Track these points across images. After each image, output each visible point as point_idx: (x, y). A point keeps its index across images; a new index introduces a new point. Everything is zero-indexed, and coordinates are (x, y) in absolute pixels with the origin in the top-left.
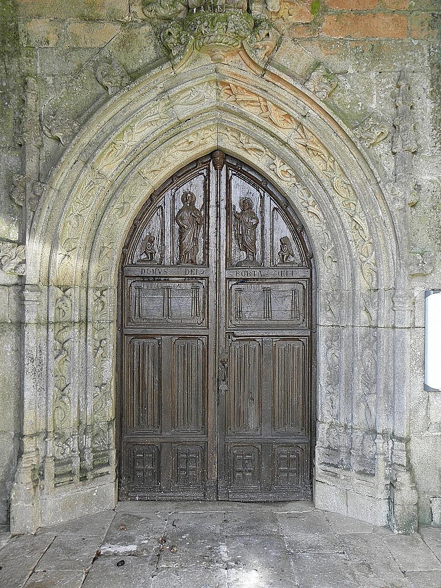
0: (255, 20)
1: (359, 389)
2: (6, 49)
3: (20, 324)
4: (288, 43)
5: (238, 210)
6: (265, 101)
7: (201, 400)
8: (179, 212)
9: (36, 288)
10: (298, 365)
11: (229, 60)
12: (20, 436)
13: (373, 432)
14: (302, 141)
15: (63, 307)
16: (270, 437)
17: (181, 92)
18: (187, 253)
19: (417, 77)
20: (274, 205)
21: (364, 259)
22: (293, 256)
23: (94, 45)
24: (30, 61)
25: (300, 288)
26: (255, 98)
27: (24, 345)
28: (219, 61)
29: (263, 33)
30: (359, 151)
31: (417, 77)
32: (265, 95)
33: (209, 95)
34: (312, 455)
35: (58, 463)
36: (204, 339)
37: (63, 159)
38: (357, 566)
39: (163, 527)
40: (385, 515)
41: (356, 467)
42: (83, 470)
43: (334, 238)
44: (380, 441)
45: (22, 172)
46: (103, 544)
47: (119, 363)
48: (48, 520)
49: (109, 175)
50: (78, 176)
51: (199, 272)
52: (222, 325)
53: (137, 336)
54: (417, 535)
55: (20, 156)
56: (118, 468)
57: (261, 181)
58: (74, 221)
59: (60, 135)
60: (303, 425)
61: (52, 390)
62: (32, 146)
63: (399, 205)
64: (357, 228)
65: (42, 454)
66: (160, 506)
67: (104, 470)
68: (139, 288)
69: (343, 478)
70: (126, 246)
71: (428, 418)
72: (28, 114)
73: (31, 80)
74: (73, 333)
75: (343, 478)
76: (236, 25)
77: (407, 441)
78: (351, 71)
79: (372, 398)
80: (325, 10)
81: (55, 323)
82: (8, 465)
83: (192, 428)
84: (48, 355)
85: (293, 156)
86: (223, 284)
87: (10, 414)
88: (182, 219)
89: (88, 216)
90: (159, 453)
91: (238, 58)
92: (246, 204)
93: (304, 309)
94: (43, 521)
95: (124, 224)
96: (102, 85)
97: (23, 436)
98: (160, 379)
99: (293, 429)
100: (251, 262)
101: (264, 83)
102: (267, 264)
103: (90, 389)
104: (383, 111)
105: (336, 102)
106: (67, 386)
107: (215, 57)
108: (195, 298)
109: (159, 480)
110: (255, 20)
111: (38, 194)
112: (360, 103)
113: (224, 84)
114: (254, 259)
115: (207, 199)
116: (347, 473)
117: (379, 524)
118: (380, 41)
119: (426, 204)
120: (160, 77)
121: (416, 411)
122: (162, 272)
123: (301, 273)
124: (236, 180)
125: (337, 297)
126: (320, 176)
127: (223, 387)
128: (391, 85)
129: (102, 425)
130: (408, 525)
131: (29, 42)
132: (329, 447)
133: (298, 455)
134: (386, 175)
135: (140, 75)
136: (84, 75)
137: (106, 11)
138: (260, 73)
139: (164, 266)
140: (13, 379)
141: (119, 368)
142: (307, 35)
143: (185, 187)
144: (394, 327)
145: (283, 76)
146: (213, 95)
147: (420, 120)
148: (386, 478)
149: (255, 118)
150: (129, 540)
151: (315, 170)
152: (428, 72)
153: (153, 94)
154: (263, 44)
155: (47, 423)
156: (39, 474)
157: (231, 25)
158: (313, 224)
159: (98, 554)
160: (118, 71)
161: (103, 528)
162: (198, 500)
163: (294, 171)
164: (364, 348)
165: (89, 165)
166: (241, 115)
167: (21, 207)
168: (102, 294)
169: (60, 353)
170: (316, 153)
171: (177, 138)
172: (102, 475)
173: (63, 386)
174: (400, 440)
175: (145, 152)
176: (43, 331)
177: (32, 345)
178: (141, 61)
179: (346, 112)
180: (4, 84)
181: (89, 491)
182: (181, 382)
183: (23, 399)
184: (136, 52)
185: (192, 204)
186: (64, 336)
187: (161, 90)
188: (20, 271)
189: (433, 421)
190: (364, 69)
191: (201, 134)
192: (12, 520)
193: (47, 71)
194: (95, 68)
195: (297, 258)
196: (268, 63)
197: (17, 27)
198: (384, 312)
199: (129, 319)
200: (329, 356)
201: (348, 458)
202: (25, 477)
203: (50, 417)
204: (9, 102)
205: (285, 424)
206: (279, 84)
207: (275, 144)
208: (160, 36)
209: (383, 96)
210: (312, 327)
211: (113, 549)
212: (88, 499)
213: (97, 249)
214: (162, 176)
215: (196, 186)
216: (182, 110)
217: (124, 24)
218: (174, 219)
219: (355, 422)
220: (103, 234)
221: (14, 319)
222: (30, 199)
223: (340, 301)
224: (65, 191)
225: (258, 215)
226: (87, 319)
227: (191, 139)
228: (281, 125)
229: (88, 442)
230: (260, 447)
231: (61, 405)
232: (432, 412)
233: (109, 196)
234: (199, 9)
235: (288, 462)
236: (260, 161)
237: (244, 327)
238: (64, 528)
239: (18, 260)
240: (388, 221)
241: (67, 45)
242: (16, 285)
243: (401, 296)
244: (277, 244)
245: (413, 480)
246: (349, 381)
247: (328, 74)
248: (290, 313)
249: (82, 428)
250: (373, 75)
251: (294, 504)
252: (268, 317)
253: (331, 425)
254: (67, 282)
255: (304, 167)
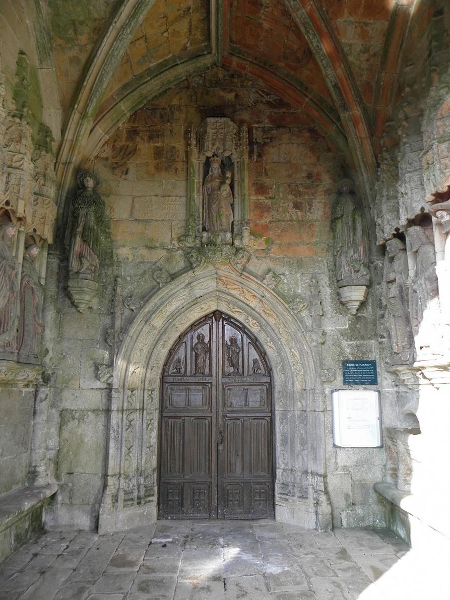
0: (236, 248)
1: (298, 447)
2: (106, 263)
3: (108, 411)
4: (254, 259)
5: (229, 343)
6: (242, 288)
7: (207, 456)
8: (195, 345)
9: (117, 390)
10: (265, 433)
11: (223, 268)
12: (105, 476)
13: (306, 472)
14: (263, 309)
15: (131, 401)
16: (248, 478)
17: (198, 284)
18: (200, 368)
19: (321, 276)
20: (249, 341)
21: (298, 372)
22: (260, 369)
23: (152, 261)
24: (118, 269)
25: (265, 388)
26: (237, 287)
27: (110, 422)
28: (218, 269)
29: (240, 256)
30: (292, 316)
31: (321, 276)
32: (242, 286)
33: (212, 285)
34: (274, 490)
35: (126, 493)
36: (209, 419)
37: (135, 321)
38: (295, 546)
39: (187, 531)
40: (314, 522)
41: (298, 494)
42: (139, 498)
43: (282, 360)
44: (310, 477)
45: (113, 326)
46: (153, 538)
47: (160, 434)
48: (120, 526)
49: (158, 327)
50: (142, 329)
51: (207, 379)
52: (220, 411)
53: (170, 417)
54: (332, 533)
55: (112, 318)
56: (158, 499)
57: (242, 329)
58: (139, 353)
59: (133, 308)
60: (268, 471)
61: (124, 449)
62: (118, 314)
63: (314, 344)
64: (294, 355)
65: (117, 487)
66: (183, 522)
67: (151, 498)
68: (172, 389)
69: (291, 501)
70: (165, 365)
71: (336, 464)
72: (117, 298)
73: (119, 279)
74: (136, 416)
75: (291, 501)
76: (226, 253)
77: (325, 476)
78: (287, 273)
79: (306, 452)
80: (273, 243)
81: (126, 410)
82: (97, 494)
83: (202, 473)
84: (122, 428)
85: (258, 315)
86: (221, 386)
87: (100, 463)
88: (197, 349)
89: (146, 350)
90: (183, 489)
91: (228, 267)
92: (233, 340)
93: (267, 401)
94: (116, 528)
95: (164, 352)
96: (156, 281)
97: (108, 476)
98: (184, 443)
99: (263, 474)
100: (236, 373)
101: (242, 279)
102: (246, 374)
103: (144, 448)
104: (305, 294)
105: (280, 289)
106: (132, 447)
107: (216, 267)
108: (204, 395)
109: (183, 506)
110: (236, 248)
111: (121, 339)
112: (292, 290)
113: (220, 279)
114: (238, 371)
115: (211, 339)
116: (294, 498)
117: (311, 527)
118: (302, 258)
119: (329, 343)
120: (186, 277)
121: (330, 459)
122: (185, 379)
123: (266, 380)
124: (227, 327)
125: (285, 394)
126: (273, 327)
127: (221, 448)
128: (308, 280)
129: (150, 471)
130: (326, 527)
131: (118, 259)
132: (283, 484)
133: (266, 490)
134: (307, 327)
135: (177, 277)
136: (147, 276)
137: (159, 243)
138: (239, 275)
139: (187, 376)
140: (102, 443)
141: (160, 437)
142: (263, 255)
143: (199, 330)
144: (315, 411)
145: (251, 277)
146: (215, 284)
147: (324, 299)
148: (314, 499)
149: (237, 296)
150: (168, 537)
151: (270, 323)
152: (327, 274)
153: (183, 285)
154: (241, 260)
155: (120, 468)
156: (115, 499)
157: (224, 253)
158: (271, 352)
159: (151, 543)
160: (165, 275)
161: (151, 532)
162: (206, 519)
163: (362, 143)
164: (300, 423)
165: (148, 323)
166: (230, 294)
167: (111, 346)
168: (151, 393)
169: (129, 427)
170: (270, 315)
171: (195, 306)
172: (149, 501)
173: (129, 447)
174: (320, 476)
175: (177, 314)
176: (120, 413)
177: (114, 422)
178: (176, 269)
179: (285, 294)
180: (104, 281)
181: (142, 511)
182: (196, 445)
183: (109, 454)
184: (174, 263)
185: (203, 340)
186: (131, 417)
187: (187, 283)
188: (109, 381)
189: (340, 465)
190: (294, 272)
191: (208, 304)
192: (99, 527)
193: (127, 274)
194: (153, 273)
195: (262, 370)
196: (243, 270)
197: (112, 252)
198: (309, 402)
199: (166, 407)
200: (281, 428)
201: (293, 489)
202: (108, 500)
203: (122, 465)
204: (106, 290)
205: (257, 471)
206: (249, 280)
207: (249, 309)
208: (187, 255)
209: (304, 286)
210: (272, 411)
211: (159, 540)
212: (141, 516)
213: (151, 365)
214: (187, 325)
215: (205, 330)
216: (198, 292)
217: (168, 250)
218: (192, 349)
219: (297, 467)
220: (153, 357)
221: (104, 408)
222: (117, 342)
223: (286, 396)
224: (135, 337)
225: (240, 346)
226: (143, 408)
227: (203, 306)
228: (251, 300)
229: (142, 481)
230: (243, 485)
231: (128, 458)
232: (339, 460)
233: (157, 338)
234: (207, 245)
235: (260, 494)
236: (241, 318)
237: (232, 412)
238: (129, 532)
239: (109, 375)
240: (309, 352)
241: (138, 261)
242: (106, 388)
243: (317, 394)
244: (251, 362)
245: (329, 499)
246: (292, 443)
247: (275, 275)
248: (259, 403)
249: (140, 472)
250: (298, 275)
251: (263, 520)
252: (246, 405)
253: (284, 470)
254: (134, 386)
255: (264, 322)
